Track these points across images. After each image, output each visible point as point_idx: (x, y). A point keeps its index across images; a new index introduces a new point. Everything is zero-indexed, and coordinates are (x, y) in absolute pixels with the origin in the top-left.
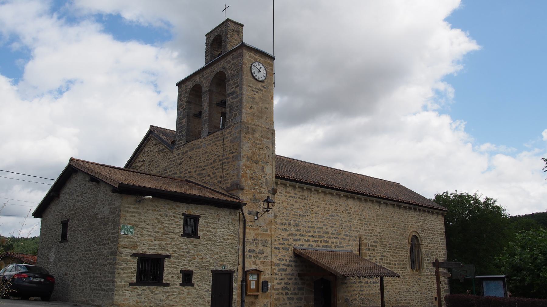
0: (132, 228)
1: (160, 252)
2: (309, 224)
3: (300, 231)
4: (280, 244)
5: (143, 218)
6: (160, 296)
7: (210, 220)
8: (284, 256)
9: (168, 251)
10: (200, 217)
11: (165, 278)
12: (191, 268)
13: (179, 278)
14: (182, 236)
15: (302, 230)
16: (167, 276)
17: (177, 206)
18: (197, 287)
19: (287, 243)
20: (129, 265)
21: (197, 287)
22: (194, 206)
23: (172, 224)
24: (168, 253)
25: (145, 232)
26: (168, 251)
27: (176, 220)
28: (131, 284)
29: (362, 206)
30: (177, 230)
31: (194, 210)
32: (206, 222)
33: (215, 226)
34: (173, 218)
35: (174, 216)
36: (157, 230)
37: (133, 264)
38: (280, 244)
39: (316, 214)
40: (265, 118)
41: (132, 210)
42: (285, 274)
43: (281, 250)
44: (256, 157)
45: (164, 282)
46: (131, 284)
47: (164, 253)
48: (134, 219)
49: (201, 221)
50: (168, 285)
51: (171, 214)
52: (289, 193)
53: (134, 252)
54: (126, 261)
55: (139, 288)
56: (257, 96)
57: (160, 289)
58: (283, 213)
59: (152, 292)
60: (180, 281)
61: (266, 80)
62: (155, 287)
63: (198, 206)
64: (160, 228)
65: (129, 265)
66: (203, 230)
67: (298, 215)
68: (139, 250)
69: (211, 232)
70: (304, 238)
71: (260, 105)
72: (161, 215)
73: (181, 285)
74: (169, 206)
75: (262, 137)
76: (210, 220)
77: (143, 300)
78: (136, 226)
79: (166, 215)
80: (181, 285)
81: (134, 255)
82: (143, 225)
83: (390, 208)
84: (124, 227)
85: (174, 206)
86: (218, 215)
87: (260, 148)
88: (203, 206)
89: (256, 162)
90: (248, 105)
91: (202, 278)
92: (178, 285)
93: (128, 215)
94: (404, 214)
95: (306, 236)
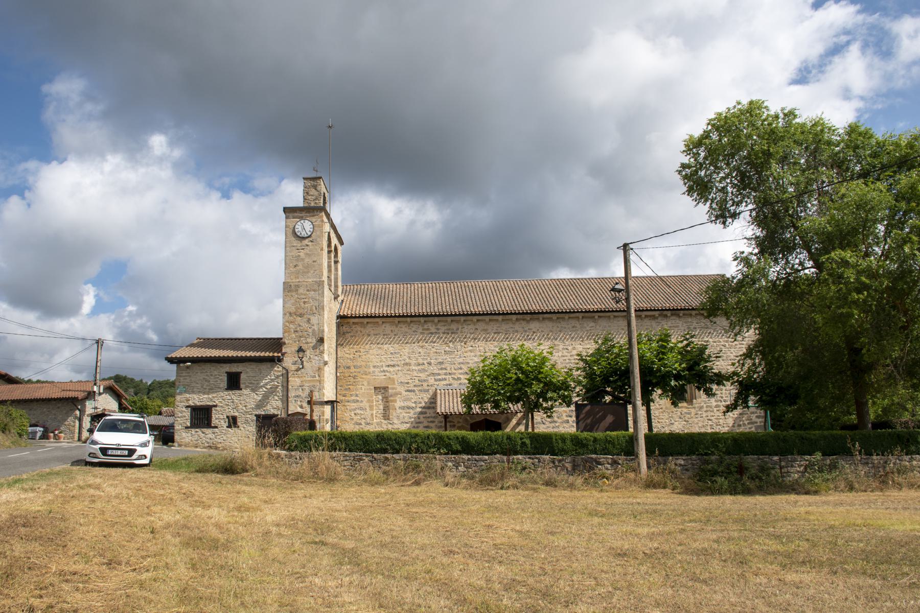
0: (184, 388)
1: (208, 403)
2: (461, 360)
3: (446, 369)
4: (415, 386)
5: (193, 379)
6: (210, 436)
7: (251, 374)
8: (422, 398)
9: (214, 402)
10: (241, 372)
11: (213, 422)
12: (236, 414)
13: (225, 422)
14: (226, 389)
15: (448, 368)
16: (214, 422)
17: (221, 367)
18: (242, 429)
19: (425, 384)
20: (184, 414)
21: (242, 429)
22: (236, 365)
23: (217, 381)
24: (215, 404)
25: (195, 390)
26: (214, 402)
27: (221, 378)
28: (187, 428)
29: (558, 327)
30: (221, 386)
31: (234, 368)
32: (247, 376)
33: (257, 378)
34: (218, 376)
35: (219, 375)
36: (205, 387)
37: (187, 413)
38: (415, 386)
39: (471, 348)
40: (312, 272)
41: (184, 374)
42: (424, 417)
43: (417, 392)
44: (301, 311)
45: (213, 425)
46: (187, 428)
47: (211, 404)
48: (186, 381)
49: (243, 376)
50: (216, 427)
51: (216, 373)
52: (428, 329)
53: (187, 404)
54: (182, 412)
55: (193, 430)
56: (302, 254)
57: (208, 431)
58: (420, 353)
59: (203, 433)
60: (227, 424)
61: (314, 234)
62: (205, 429)
63: (239, 364)
64: (207, 385)
65: (184, 414)
66: (245, 383)
67: (443, 352)
68: (191, 403)
69: (254, 384)
70: (453, 376)
71: (307, 260)
72: (207, 375)
73: (227, 427)
74: (214, 368)
75: (308, 290)
76: (251, 374)
77: (196, 439)
78: (187, 385)
79: (212, 375)
80: (227, 427)
81: (187, 407)
82: (193, 384)
83: (619, 321)
84: (178, 388)
85: (219, 367)
86: (260, 369)
87: (305, 303)
88: (244, 364)
89: (301, 315)
90: (291, 265)
91: (247, 422)
92: (225, 428)
93: (182, 378)
94: (652, 326)
95: (455, 374)
